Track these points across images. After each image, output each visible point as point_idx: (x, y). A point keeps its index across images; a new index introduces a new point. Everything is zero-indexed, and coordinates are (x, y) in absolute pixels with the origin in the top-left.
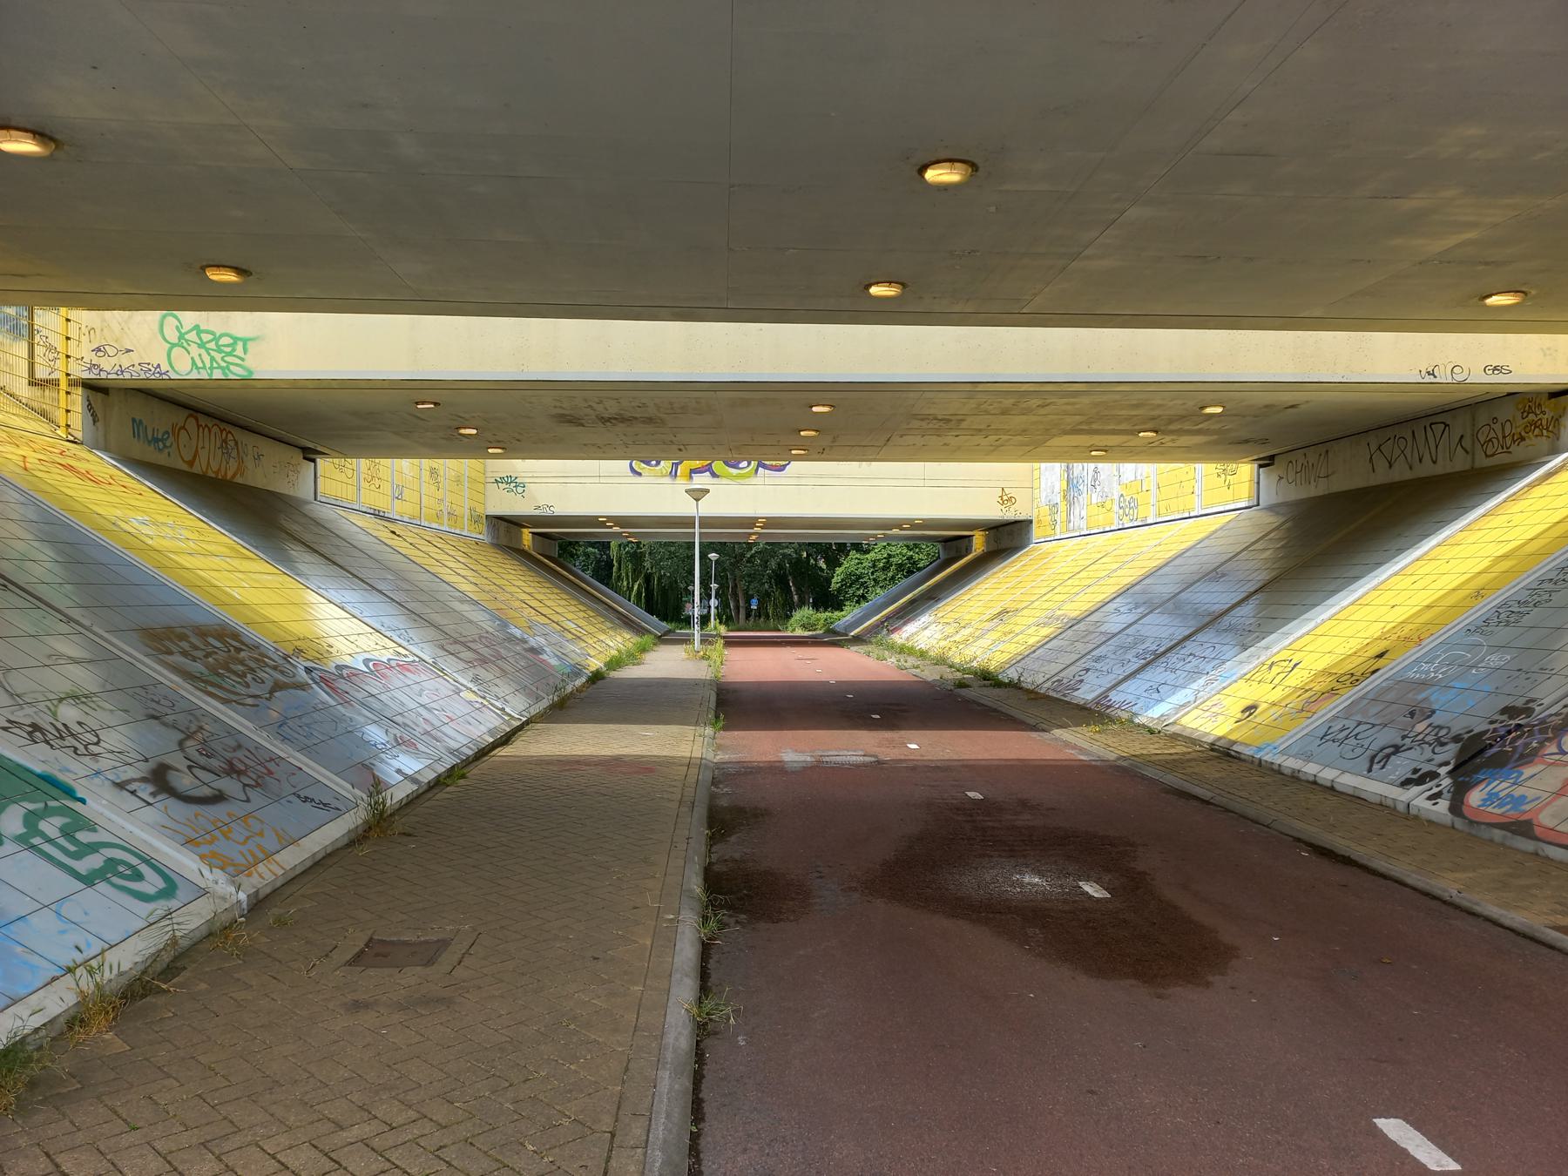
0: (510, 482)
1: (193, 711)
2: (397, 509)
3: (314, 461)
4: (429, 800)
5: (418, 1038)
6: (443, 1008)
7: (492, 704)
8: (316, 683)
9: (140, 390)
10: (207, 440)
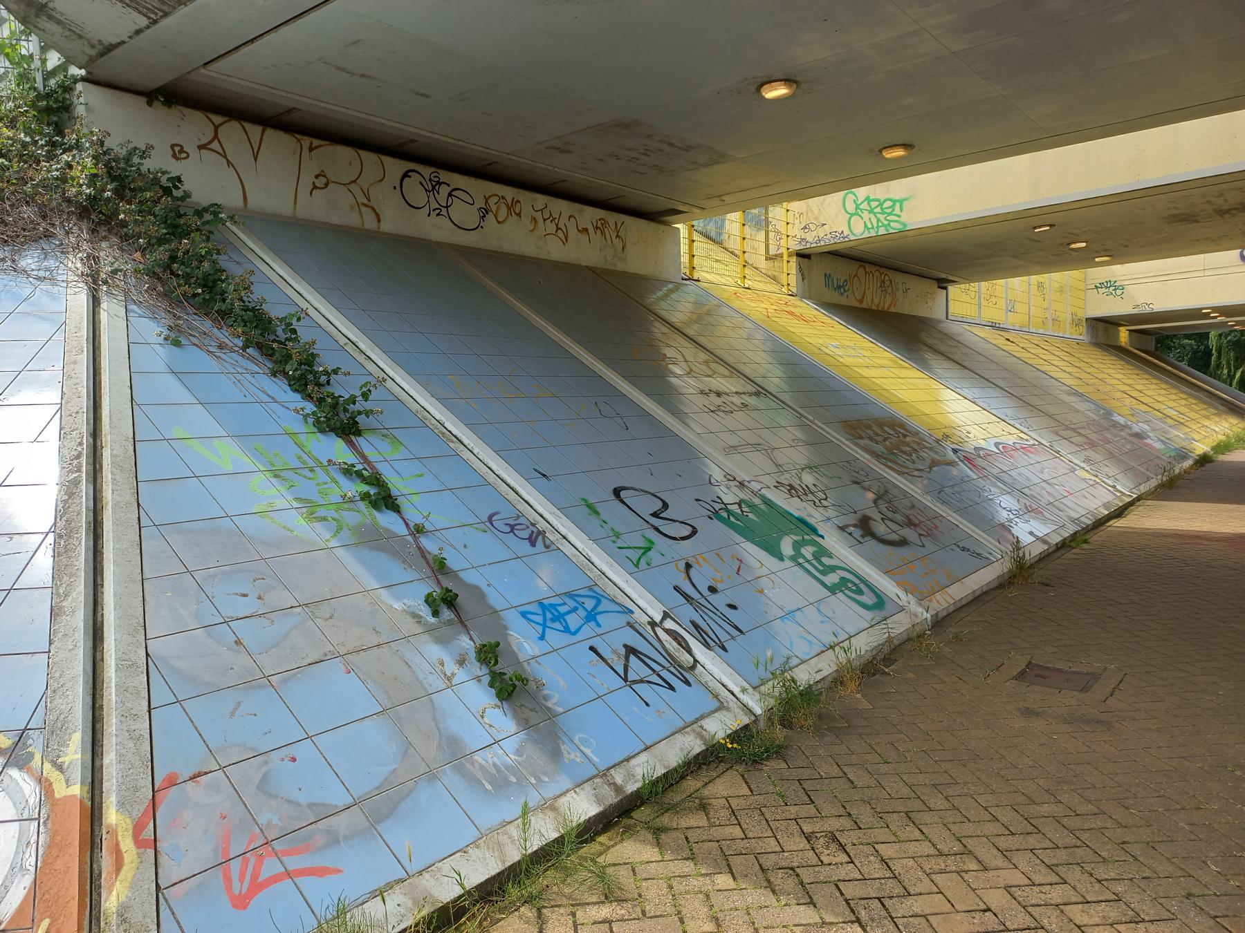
0: (1111, 287)
1: (881, 479)
2: (1011, 320)
3: (945, 288)
4: (1059, 558)
5: (1085, 749)
6: (1104, 729)
7: (1104, 482)
8: (961, 461)
9: (829, 253)
10: (871, 282)
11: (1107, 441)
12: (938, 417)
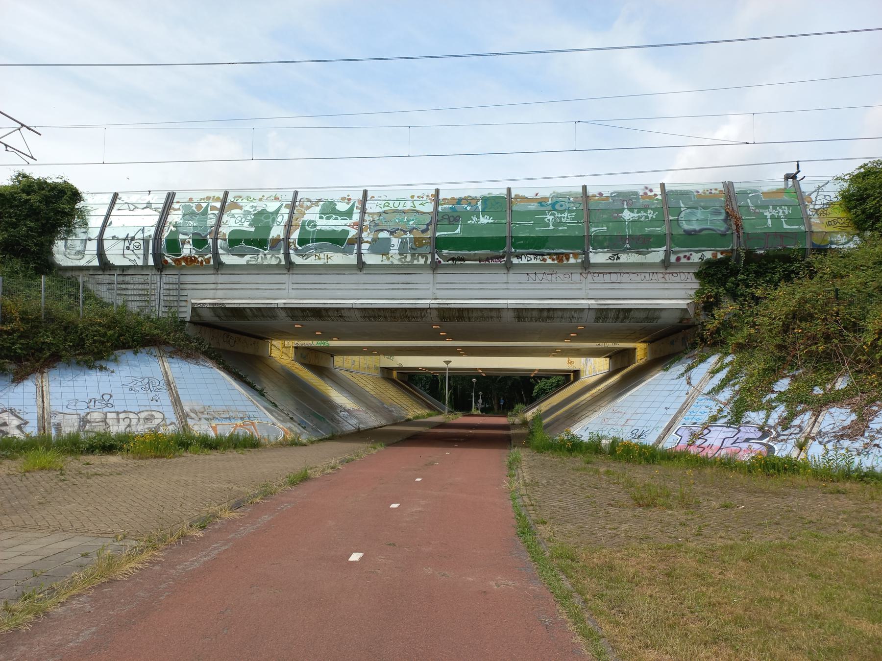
11: (380, 411)
12: (99, 293)
